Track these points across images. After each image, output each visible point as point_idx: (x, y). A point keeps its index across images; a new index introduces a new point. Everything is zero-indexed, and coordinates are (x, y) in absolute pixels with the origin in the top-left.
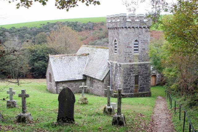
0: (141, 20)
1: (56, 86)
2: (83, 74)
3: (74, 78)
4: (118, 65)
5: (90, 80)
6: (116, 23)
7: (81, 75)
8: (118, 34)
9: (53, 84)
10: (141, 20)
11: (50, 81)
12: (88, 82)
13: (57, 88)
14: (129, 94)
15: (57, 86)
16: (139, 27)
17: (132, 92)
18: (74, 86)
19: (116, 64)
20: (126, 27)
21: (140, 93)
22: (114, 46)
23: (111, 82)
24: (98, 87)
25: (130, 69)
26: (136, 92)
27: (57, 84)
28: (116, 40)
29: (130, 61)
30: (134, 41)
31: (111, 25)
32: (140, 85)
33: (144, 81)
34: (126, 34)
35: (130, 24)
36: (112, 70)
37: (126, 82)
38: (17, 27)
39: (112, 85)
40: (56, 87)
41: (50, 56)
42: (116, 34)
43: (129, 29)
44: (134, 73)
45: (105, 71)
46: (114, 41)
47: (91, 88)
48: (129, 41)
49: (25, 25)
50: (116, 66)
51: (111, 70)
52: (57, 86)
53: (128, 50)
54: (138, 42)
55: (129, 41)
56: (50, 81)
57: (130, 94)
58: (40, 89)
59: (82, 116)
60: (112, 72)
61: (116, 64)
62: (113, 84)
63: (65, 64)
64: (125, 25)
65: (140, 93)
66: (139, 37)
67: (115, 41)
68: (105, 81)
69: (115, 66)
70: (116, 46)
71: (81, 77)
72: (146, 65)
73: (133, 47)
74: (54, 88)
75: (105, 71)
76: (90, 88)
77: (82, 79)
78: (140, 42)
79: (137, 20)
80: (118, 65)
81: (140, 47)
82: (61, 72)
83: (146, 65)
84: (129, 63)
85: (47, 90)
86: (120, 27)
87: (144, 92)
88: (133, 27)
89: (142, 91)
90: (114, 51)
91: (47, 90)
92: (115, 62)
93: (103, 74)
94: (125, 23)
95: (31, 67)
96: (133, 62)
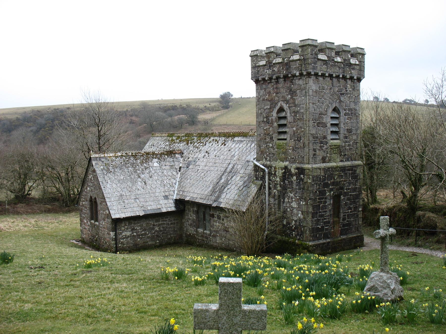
0: (345, 60)
1: (114, 229)
2: (175, 198)
4: (293, 171)
5: (197, 212)
6: (287, 64)
8: (292, 93)
9: (104, 224)
10: (345, 60)
11: (94, 215)
12: (191, 216)
13: (116, 235)
15: (116, 231)
20: (316, 75)
22: (275, 124)
25: (324, 180)
27: (116, 226)
28: (285, 107)
29: (324, 160)
30: (330, 110)
31: (269, 72)
32: (344, 219)
33: (350, 208)
34: (316, 92)
35: (325, 66)
36: (269, 184)
37: (317, 210)
40: (112, 234)
42: (284, 92)
43: (321, 79)
44: (332, 190)
46: (276, 110)
47: (200, 230)
48: (321, 108)
50: (285, 173)
51: (77, 199)
52: (116, 231)
53: (321, 131)
54: (339, 113)
55: (321, 108)
56: (94, 215)
57: (324, 241)
58: (62, 240)
59: (153, 286)
60: (270, 188)
64: (314, 68)
66: (341, 101)
69: (280, 173)
70: (283, 122)
71: (168, 206)
73: (329, 125)
74: (107, 236)
76: (197, 231)
77: (173, 209)
78: (342, 113)
79: (339, 59)
81: (342, 125)
84: (323, 165)
85: (83, 241)
86: (301, 75)
87: (351, 236)
88: (331, 76)
89: (346, 234)
90: (275, 136)
91: (83, 241)
94: (315, 63)
95: (41, 273)
96: (329, 161)
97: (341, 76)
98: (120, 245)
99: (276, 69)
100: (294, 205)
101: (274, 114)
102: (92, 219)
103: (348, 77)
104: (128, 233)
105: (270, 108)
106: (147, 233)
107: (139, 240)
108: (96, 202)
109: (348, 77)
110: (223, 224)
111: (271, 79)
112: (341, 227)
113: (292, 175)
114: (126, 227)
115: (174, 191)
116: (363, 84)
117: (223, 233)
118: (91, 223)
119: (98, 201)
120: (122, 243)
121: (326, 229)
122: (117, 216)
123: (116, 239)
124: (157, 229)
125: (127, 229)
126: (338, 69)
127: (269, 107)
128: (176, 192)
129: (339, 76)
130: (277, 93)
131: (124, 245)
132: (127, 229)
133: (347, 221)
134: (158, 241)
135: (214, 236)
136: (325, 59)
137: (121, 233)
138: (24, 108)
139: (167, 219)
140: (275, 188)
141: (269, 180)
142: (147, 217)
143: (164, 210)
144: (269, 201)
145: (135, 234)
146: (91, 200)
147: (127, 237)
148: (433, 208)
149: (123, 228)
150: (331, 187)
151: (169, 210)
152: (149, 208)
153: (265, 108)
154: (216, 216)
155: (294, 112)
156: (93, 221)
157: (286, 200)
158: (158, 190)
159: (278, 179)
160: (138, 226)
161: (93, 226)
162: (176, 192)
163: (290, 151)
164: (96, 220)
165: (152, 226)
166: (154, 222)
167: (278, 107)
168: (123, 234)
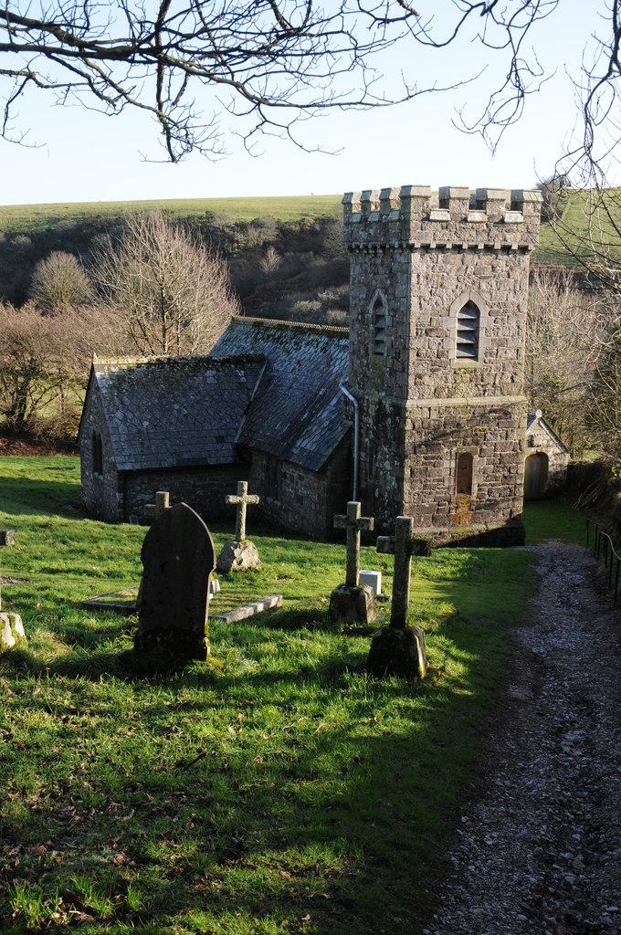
4: (388, 409)
9: (109, 478)
13: (124, 498)
15: (125, 493)
19: (380, 403)
24: (300, 499)
29: (437, 393)
36: (360, 428)
46: (372, 304)
52: (125, 493)
54: (477, 312)
62: (363, 485)
68: (329, 473)
77: (230, 460)
80: (388, 409)
90: (370, 346)
99: (371, 231)
100: (387, 465)
101: (371, 308)
102: (95, 470)
103: (498, 246)
105: (366, 299)
108: (100, 441)
109: (498, 246)
110: (297, 490)
111: (366, 247)
117: (296, 505)
118: (94, 476)
119: (103, 442)
124: (200, 492)
126: (474, 233)
128: (240, 431)
129: (477, 246)
132: (146, 489)
133: (488, 500)
135: (286, 511)
136: (445, 219)
137: (135, 497)
138: (36, 210)
139: (219, 477)
140: (368, 436)
141: (360, 420)
143: (212, 461)
144: (359, 456)
146: (94, 438)
149: (138, 488)
152: (186, 456)
153: (361, 296)
154: (288, 476)
155: (393, 309)
156: (96, 474)
157: (379, 456)
158: (207, 426)
159: (371, 421)
161: (96, 481)
162: (240, 431)
164: (100, 473)
165: (190, 488)
167: (375, 299)
168: (139, 497)
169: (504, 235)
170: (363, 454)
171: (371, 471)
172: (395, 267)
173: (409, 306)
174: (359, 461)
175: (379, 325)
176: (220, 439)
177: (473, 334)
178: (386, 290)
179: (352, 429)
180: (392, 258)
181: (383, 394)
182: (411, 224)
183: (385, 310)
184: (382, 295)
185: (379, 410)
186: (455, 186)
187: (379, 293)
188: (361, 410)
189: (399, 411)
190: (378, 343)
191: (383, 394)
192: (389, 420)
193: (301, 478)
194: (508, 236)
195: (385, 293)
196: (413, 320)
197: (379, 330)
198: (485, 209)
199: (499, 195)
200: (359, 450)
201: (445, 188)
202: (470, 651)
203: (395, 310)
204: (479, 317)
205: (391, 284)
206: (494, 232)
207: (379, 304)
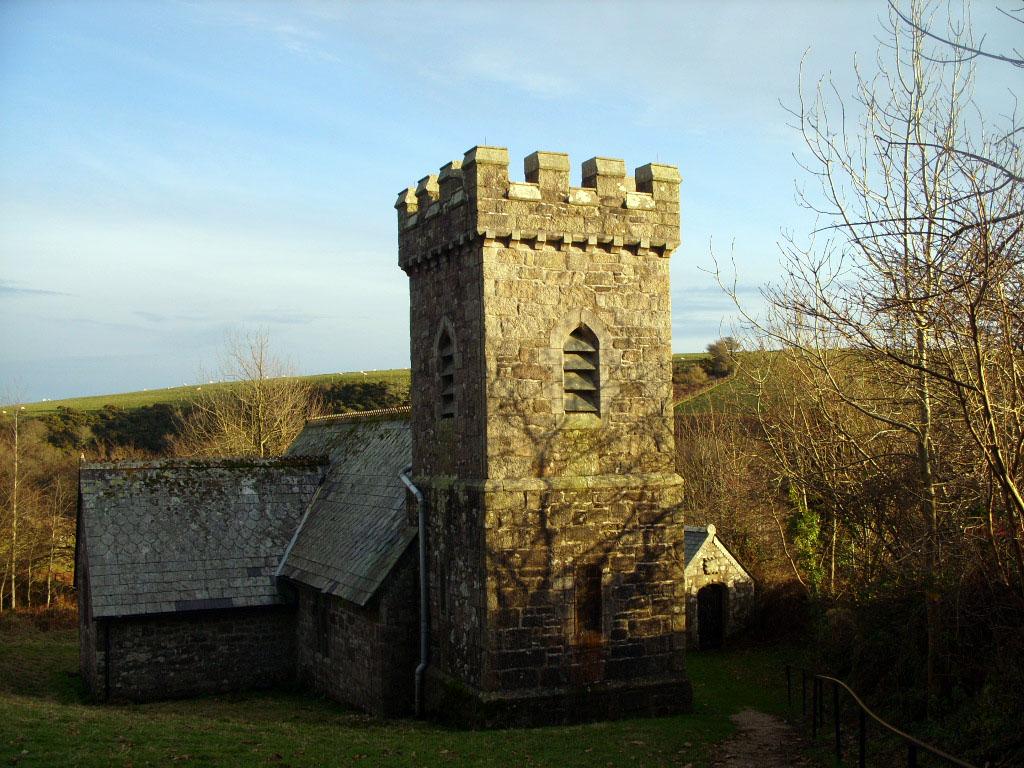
1: (104, 645)
3: (215, 594)
4: (463, 498)
7: (268, 582)
13: (107, 659)
14: (533, 693)
16: (593, 241)
17: (559, 684)
18: (223, 649)
19: (450, 492)
21: (612, 685)
22: (437, 377)
23: (423, 618)
24: (351, 653)
26: (500, 648)
38: (123, 405)
39: (428, 634)
40: (99, 655)
41: (734, 717)
45: (392, 543)
49: (160, 399)
61: (450, 492)
62: (435, 627)
63: (170, 516)
65: (612, 685)
67: (446, 341)
68: (383, 610)
69: (442, 507)
71: (256, 592)
72: (653, 499)
75: (392, 543)
77: (266, 600)
78: (604, 340)
80: (463, 498)
81: (604, 376)
82: (141, 558)
83: (653, 499)
87: (643, 683)
90: (438, 405)
92: (444, 481)
93: (379, 565)
97: (593, 241)
98: (118, 685)
104: (143, 657)
106: (196, 658)
107: (172, 674)
112: (606, 658)
113: (460, 510)
114: (137, 640)
115: (280, 558)
116: (675, 264)
120: (125, 681)
121: (551, 659)
122: (111, 612)
123: (106, 671)
125: (140, 645)
126: (580, 221)
127: (427, 334)
130: (439, 296)
131: (130, 684)
133: (630, 640)
134: (225, 681)
137: (122, 656)
141: (427, 523)
142: (189, 617)
143: (240, 602)
144: (427, 580)
145: (161, 659)
147: (137, 666)
148: (430, 599)
149: (128, 644)
150: (563, 543)
151: (254, 602)
152: (199, 596)
157: (453, 578)
159: (440, 523)
160: (170, 640)
163: (459, 445)
166: (214, 633)
167: (439, 333)
168: (129, 658)
169: (627, 226)
170: (432, 576)
171: (444, 603)
172: (463, 275)
173: (482, 330)
174: (428, 589)
175: (448, 372)
176: (254, 572)
177: (592, 375)
178: (452, 315)
179: (416, 537)
180: (458, 264)
181: (456, 477)
182: (479, 203)
183: (454, 349)
184: (449, 324)
185: (449, 503)
186: (546, 151)
187: (446, 323)
188: (427, 507)
189: (477, 501)
190: (449, 398)
191: (456, 477)
192: (464, 515)
193: (351, 620)
194: (634, 228)
195: (453, 320)
196: (490, 353)
197: (449, 379)
198: (595, 186)
199: (614, 168)
200: (427, 571)
201: (531, 156)
202: (701, 632)
203: (465, 341)
204: (597, 349)
205: (459, 305)
206: (614, 221)
207: (446, 341)
